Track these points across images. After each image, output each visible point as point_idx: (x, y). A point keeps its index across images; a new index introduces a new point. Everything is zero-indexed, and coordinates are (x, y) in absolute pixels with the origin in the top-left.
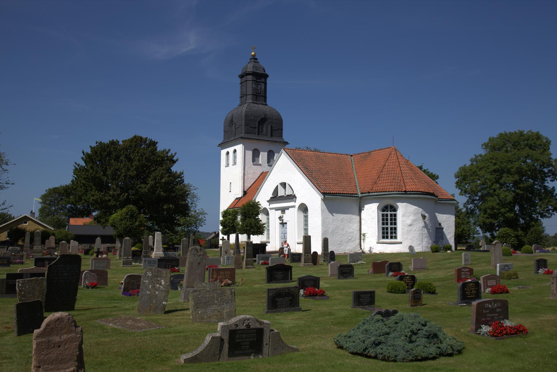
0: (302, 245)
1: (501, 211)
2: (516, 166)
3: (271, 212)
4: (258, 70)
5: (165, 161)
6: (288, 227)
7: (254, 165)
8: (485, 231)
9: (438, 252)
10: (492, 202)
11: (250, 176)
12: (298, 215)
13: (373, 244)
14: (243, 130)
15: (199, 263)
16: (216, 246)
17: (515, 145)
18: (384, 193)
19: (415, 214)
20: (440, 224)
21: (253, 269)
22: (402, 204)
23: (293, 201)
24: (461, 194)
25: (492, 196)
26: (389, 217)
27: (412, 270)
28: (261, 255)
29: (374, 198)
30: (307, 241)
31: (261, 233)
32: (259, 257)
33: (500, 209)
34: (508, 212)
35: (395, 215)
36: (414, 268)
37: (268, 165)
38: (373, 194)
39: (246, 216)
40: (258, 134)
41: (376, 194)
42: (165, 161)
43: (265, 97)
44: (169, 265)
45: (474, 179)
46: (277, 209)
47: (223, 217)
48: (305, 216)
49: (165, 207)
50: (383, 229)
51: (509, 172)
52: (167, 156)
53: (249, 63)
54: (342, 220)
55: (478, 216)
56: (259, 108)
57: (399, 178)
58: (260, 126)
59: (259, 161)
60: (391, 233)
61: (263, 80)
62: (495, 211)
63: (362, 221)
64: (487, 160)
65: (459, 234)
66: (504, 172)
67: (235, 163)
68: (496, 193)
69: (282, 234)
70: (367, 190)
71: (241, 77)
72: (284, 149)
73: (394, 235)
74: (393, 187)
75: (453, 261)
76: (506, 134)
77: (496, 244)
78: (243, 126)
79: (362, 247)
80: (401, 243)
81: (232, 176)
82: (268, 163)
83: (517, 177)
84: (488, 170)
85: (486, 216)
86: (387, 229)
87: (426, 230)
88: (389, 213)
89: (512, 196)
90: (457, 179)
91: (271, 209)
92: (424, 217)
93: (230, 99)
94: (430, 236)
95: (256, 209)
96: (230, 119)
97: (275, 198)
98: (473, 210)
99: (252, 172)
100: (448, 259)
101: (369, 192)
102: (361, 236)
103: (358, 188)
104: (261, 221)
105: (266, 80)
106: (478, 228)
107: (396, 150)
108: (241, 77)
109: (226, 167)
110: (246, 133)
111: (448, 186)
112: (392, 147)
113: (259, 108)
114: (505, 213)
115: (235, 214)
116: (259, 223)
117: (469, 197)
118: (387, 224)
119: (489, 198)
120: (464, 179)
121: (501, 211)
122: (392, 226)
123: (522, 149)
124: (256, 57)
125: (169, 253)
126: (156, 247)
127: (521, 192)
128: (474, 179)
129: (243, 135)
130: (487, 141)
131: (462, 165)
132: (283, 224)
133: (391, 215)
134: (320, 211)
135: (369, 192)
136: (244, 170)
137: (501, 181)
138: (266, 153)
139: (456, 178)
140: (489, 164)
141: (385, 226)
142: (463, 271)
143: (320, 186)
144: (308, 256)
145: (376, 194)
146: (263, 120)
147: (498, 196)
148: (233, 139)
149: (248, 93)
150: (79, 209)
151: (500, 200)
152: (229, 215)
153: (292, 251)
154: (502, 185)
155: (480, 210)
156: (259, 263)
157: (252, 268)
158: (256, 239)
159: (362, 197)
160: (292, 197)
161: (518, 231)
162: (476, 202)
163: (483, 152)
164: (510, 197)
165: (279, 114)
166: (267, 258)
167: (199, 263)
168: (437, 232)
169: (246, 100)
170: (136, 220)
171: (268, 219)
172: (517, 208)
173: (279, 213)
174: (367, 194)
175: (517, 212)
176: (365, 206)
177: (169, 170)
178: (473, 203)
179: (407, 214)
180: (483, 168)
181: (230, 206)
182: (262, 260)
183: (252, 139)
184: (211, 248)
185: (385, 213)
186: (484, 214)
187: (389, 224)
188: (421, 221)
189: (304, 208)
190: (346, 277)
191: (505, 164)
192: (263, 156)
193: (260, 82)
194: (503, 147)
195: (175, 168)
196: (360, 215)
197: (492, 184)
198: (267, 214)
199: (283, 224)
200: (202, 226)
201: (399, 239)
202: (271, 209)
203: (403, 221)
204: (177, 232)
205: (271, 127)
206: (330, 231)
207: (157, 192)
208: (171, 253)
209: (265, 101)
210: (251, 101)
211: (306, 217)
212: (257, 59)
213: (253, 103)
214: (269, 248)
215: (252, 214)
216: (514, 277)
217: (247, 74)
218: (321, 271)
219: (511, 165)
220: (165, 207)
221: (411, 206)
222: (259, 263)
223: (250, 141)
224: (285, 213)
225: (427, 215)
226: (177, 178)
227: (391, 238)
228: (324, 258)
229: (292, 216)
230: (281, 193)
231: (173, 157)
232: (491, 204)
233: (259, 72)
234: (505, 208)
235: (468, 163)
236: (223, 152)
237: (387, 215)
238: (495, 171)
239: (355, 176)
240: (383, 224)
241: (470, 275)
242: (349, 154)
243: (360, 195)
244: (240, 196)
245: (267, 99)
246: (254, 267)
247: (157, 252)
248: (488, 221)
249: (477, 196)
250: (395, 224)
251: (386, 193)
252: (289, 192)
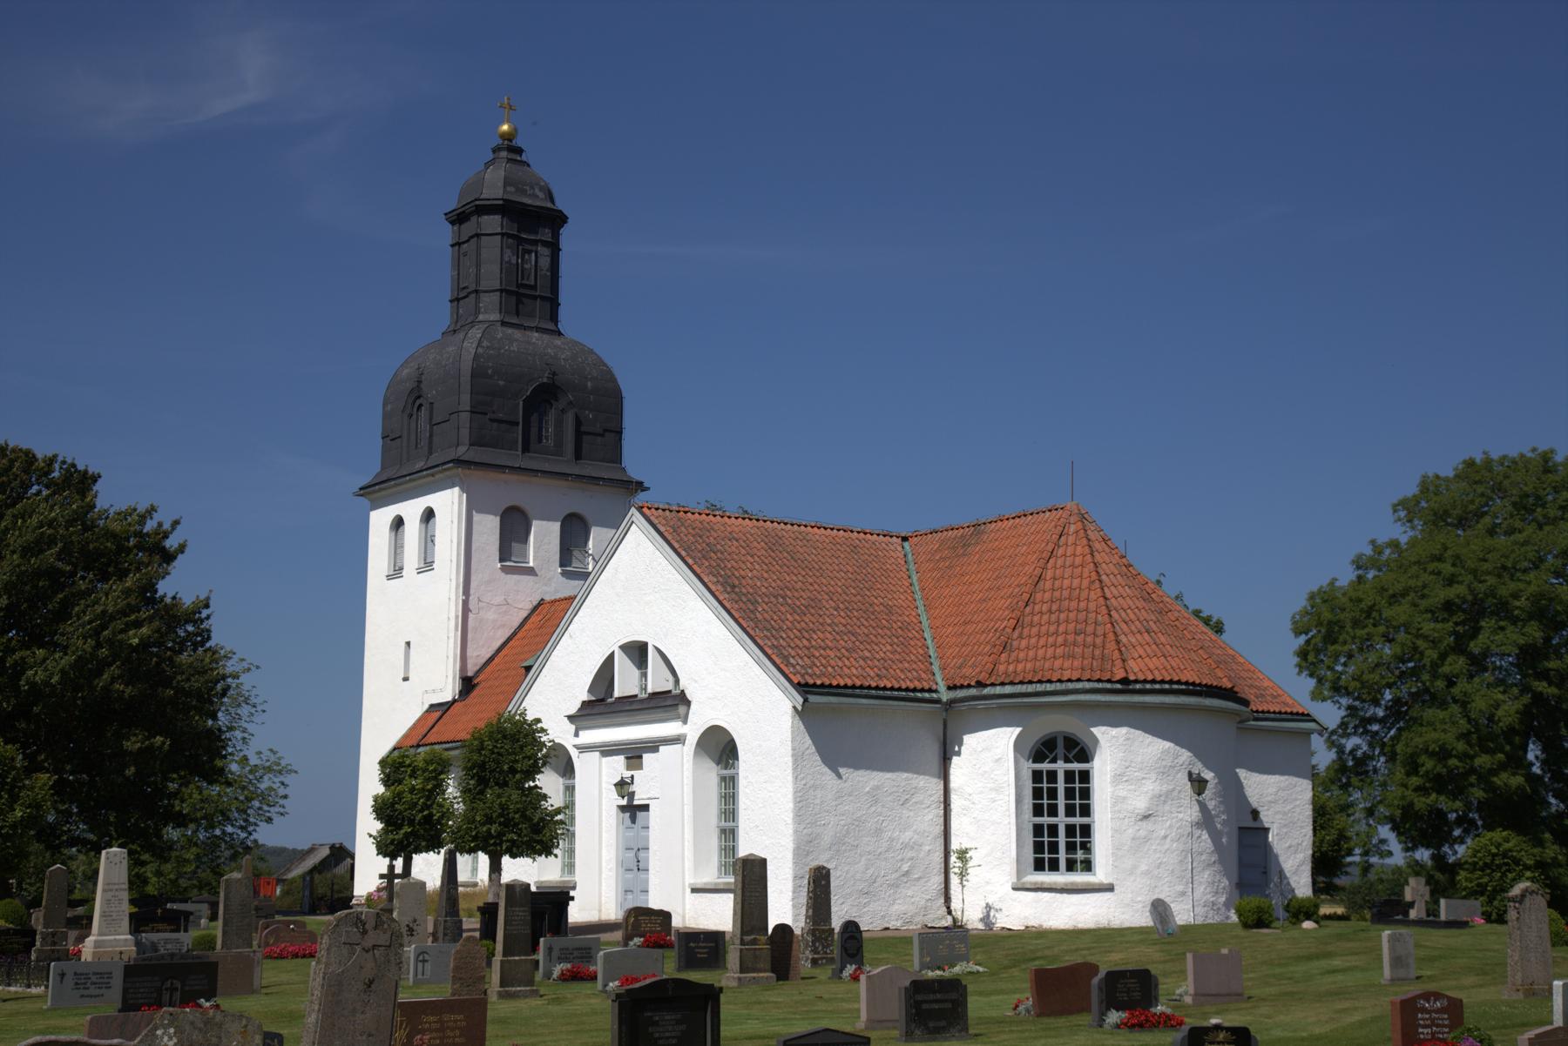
0: (731, 896)
1: (1478, 762)
2: (1533, 588)
3: (584, 765)
4: (524, 192)
5: (129, 551)
6: (652, 823)
7: (505, 570)
8: (1411, 845)
9: (1268, 926)
10: (1440, 728)
11: (491, 615)
12: (694, 774)
13: (996, 889)
14: (465, 432)
15: (371, 982)
16: (340, 897)
17: (1525, 506)
18: (1040, 688)
19: (1164, 773)
20: (1255, 814)
21: (535, 1002)
22: (1114, 731)
23: (676, 718)
24: (1316, 696)
25: (1437, 701)
26: (1061, 785)
27: (1188, 1000)
28: (560, 942)
29: (1001, 707)
30: (750, 879)
31: (546, 849)
32: (550, 949)
33: (1472, 758)
34: (1503, 767)
35: (1085, 776)
36: (1196, 995)
37: (564, 574)
38: (998, 690)
39: (483, 777)
40: (526, 449)
41: (1008, 689)
42: (129, 551)
43: (553, 303)
44: (173, 990)
45: (1369, 637)
46: (608, 750)
47: (387, 781)
48: (723, 779)
49: (132, 744)
50: (1038, 830)
51: (1503, 610)
52: (139, 534)
53: (487, 165)
54: (874, 796)
55: (1384, 785)
56: (527, 343)
57: (1100, 631)
58: (534, 418)
59: (525, 555)
60: (1071, 847)
61: (545, 234)
62: (1453, 762)
63: (954, 797)
64: (1418, 563)
65: (1323, 854)
66: (1482, 613)
67: (427, 564)
68: (1455, 691)
69: (638, 850)
70: (970, 674)
71: (457, 219)
72: (640, 509)
73: (1080, 855)
74: (1077, 663)
75: (1337, 962)
76: (1488, 463)
77: (1523, 896)
78: (465, 417)
79: (956, 904)
80: (1110, 888)
81: (415, 610)
82: (561, 565)
83: (1534, 632)
84: (1424, 603)
85: (1415, 781)
86: (1053, 830)
87: (1205, 836)
88: (1061, 767)
89: (1518, 705)
90: (1303, 638)
91: (583, 749)
92: (1198, 784)
93: (413, 310)
94: (1221, 861)
95: (528, 751)
96: (410, 385)
97: (601, 704)
98: (1367, 757)
99: (499, 599)
100: (1317, 957)
101: (980, 684)
102: (951, 861)
103: (936, 668)
104: (545, 797)
105: (556, 236)
106: (1385, 831)
107: (1083, 518)
108: (457, 219)
109: (389, 577)
110: (476, 442)
111: (1274, 666)
112: (1070, 505)
113: (527, 343)
114: (1493, 772)
115: (437, 770)
116: (536, 807)
117: (1349, 708)
119: (1430, 713)
120: (1330, 638)
121: (1478, 762)
122: (1071, 820)
123: (1554, 521)
124: (518, 142)
125: (154, 937)
126: (103, 915)
127: (1553, 690)
128: (1369, 637)
129: (462, 450)
130: (1411, 489)
131: (1319, 581)
132: (633, 810)
133: (1069, 776)
134: (789, 760)
135: (980, 684)
136: (466, 591)
137: (1475, 647)
138: (556, 527)
139: (1297, 633)
140: (1426, 577)
142: (1424, 1010)
143: (786, 658)
144: (754, 942)
145: (1008, 689)
146: (546, 394)
147: (1464, 705)
149: (484, 285)
151: (1469, 721)
152: (413, 775)
154: (1478, 663)
155: (1392, 758)
156: (548, 975)
157: (525, 995)
158: (521, 870)
159: (952, 702)
160: (672, 702)
161: (1540, 843)
162: (1375, 727)
163: (1402, 534)
164: (1509, 710)
165: (609, 372)
166: (587, 954)
167: (371, 982)
168: (1246, 848)
169: (477, 311)
170: (14, 798)
171: (570, 789)
172: (1533, 752)
173: (616, 766)
174: (973, 692)
175: (1536, 770)
176: (967, 739)
177: (147, 592)
178: (1366, 732)
179: (1131, 771)
180: (1404, 594)
181: (406, 736)
182: (561, 960)
183: (500, 468)
184: (313, 911)
185: (1045, 766)
186: (1408, 774)
187: (1061, 810)
188: (1186, 802)
189: (720, 748)
190: (935, 1033)
191: (1491, 580)
192: (543, 538)
193: (535, 242)
194: (1480, 515)
195: (177, 585)
196: (945, 777)
197: (1443, 657)
198: (568, 770)
199: (633, 810)
200: (269, 820)
201: (1100, 875)
202: (583, 749)
203: (1118, 800)
204: (171, 846)
205: (578, 422)
206: (827, 839)
207: (100, 683)
208: (165, 941)
209: (554, 318)
210: (495, 316)
211: (729, 785)
212: (519, 151)
213: (503, 323)
214: (577, 913)
215: (513, 771)
217: (483, 209)
218: (821, 1006)
219: (1513, 586)
220: (132, 744)
221: (1149, 738)
222: (548, 975)
223: (492, 475)
224: (640, 767)
225: (1208, 775)
226: (184, 624)
227: (1071, 866)
228: (815, 951)
229: (674, 778)
230: (626, 682)
231: (166, 536)
232: (1435, 735)
233: (529, 201)
234: (1491, 752)
235: (1346, 576)
236: (380, 519)
237: (1052, 776)
238: (1448, 606)
239: (924, 618)
240: (1038, 811)
241: (1452, 1027)
242: (894, 530)
243: (945, 696)
244: (447, 696)
245: (563, 312)
246: (535, 993)
247: (108, 936)
248: (1421, 803)
249: (1376, 703)
250: (1086, 811)
251: (1049, 687)
252: (658, 680)
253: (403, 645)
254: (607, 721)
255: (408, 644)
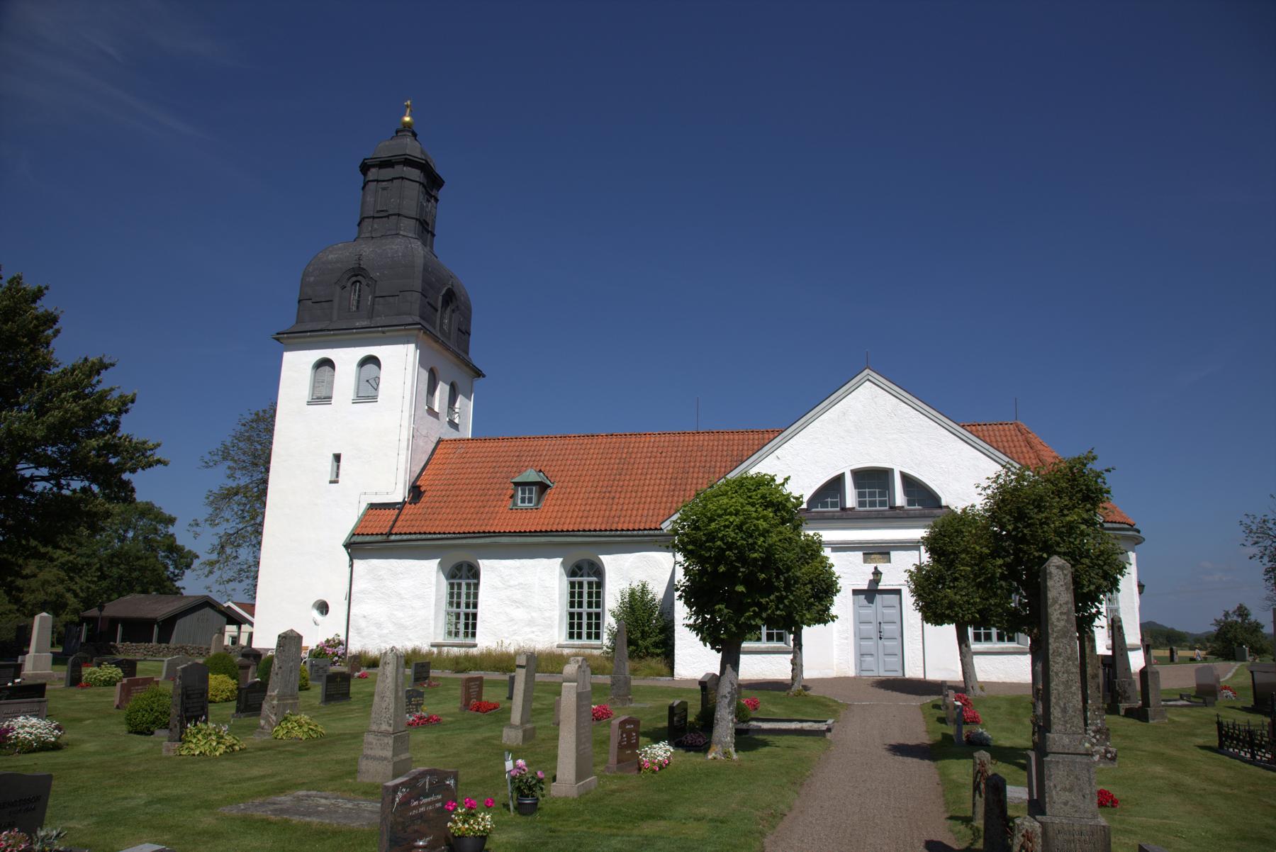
50: (572, 615)
88: (585, 580)
118: (580, 605)
141: (594, 610)
148: (365, 323)
150: (50, 457)
153: (255, 645)
187: (585, 604)
216: (474, 689)
227: (589, 636)
237: (581, 584)
240: (572, 605)
253: (331, 457)
254: (862, 525)
255: (337, 458)
